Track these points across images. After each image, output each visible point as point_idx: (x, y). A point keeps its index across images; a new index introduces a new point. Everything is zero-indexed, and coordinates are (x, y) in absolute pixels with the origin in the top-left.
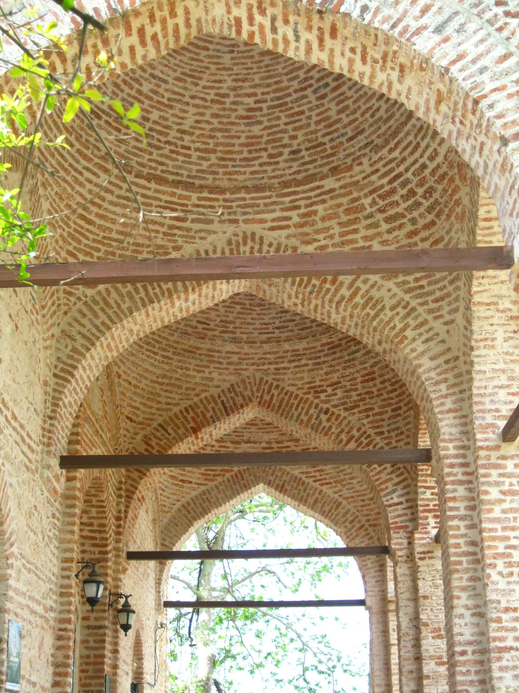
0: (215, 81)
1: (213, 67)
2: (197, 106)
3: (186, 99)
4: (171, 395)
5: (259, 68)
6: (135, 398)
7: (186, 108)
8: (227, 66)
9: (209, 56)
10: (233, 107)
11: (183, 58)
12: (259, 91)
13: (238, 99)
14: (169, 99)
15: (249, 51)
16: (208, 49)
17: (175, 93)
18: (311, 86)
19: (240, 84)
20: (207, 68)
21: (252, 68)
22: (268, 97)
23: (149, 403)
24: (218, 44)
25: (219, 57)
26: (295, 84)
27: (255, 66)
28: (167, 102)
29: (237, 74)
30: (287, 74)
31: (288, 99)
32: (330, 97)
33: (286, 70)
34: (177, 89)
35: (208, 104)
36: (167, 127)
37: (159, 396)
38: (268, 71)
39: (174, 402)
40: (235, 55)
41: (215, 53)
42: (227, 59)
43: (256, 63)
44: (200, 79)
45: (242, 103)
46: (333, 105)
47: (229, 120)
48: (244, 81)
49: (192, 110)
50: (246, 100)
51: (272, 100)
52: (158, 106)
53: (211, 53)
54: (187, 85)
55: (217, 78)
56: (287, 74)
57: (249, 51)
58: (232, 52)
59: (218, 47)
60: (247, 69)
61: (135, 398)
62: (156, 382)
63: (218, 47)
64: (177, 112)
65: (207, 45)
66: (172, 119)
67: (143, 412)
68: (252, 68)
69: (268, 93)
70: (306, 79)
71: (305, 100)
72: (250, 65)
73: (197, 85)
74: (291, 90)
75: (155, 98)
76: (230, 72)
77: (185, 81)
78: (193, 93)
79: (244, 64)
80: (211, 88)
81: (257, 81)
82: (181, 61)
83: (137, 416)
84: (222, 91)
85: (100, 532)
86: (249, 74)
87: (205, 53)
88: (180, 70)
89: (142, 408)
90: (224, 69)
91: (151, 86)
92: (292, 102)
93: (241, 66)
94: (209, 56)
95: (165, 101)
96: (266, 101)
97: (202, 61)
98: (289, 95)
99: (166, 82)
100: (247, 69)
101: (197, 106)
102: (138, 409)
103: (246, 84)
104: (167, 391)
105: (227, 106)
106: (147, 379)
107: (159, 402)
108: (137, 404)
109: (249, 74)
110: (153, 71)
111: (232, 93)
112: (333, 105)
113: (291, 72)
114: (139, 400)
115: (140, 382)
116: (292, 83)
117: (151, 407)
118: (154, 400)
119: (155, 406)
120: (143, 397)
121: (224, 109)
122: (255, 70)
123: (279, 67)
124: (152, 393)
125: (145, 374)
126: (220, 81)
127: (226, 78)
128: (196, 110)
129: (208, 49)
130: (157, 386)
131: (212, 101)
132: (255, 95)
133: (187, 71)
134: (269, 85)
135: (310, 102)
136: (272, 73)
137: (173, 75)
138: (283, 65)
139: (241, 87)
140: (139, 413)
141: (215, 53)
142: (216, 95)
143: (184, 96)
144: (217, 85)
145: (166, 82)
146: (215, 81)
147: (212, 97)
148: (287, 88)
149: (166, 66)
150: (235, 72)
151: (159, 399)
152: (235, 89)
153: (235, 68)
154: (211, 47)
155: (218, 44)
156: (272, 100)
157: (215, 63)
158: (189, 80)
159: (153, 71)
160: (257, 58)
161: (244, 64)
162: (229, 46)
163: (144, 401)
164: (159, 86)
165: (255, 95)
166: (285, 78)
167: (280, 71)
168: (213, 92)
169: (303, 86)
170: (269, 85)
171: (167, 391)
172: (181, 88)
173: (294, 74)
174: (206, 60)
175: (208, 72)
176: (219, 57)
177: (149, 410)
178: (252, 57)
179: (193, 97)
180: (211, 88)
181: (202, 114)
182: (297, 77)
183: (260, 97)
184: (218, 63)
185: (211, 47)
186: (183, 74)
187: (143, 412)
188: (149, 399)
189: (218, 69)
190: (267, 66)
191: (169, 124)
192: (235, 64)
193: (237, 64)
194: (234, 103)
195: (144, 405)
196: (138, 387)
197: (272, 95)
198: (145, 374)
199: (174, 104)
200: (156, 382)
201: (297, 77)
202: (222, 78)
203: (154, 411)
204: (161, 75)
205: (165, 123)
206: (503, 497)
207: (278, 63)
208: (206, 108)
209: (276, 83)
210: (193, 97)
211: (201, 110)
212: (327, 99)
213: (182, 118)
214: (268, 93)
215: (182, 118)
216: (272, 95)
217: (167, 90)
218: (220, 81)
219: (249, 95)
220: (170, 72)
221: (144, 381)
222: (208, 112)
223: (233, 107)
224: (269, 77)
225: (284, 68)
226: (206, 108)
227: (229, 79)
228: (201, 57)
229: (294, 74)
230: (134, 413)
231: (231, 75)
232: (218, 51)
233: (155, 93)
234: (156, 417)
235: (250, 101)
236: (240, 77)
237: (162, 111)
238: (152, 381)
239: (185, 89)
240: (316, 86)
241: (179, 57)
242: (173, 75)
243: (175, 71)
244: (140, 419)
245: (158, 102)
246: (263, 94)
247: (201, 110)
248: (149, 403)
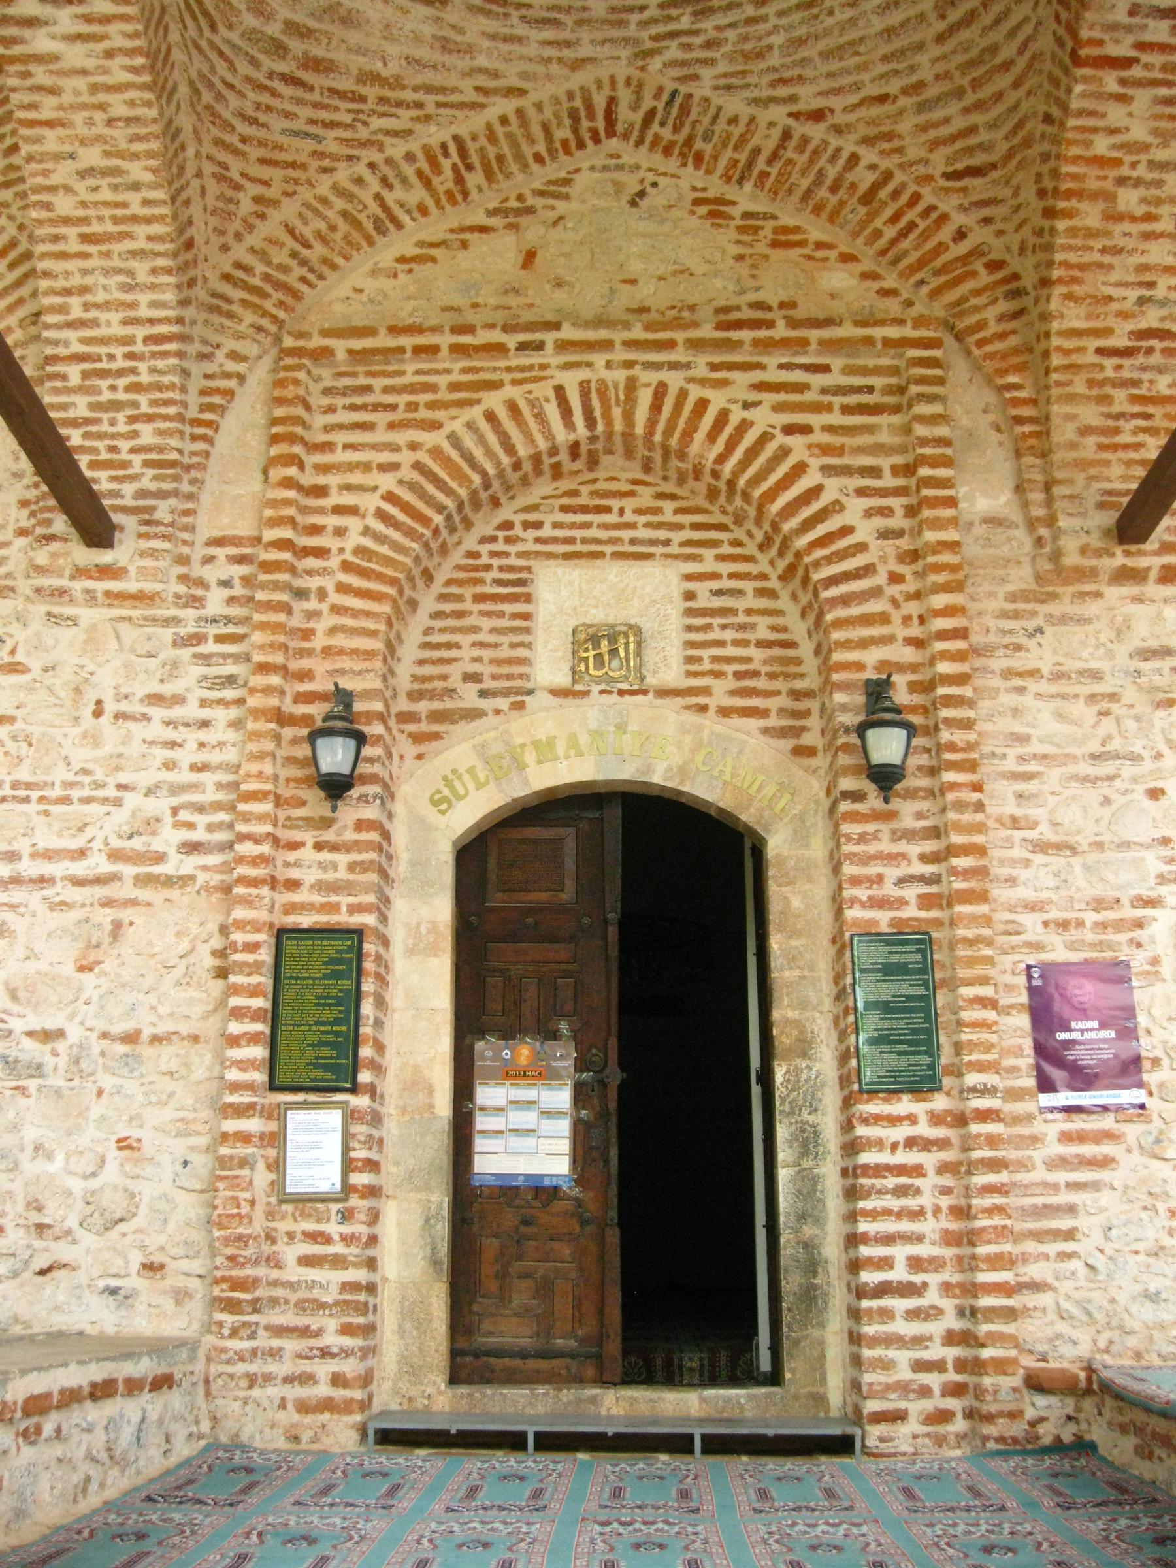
4: (1013, 21)
6: (937, 115)
23: (987, 91)
37: (993, 49)
39: (1028, 30)
47: (875, 892)
61: (937, 115)
62: (953, 29)
67: (993, 126)
83: (983, 147)
85: (808, 194)
89: (978, 118)
102: (972, 130)
104: (997, 22)
106: (920, 47)
107: (1007, 65)
108: (959, 123)
114: (953, 109)
115: (912, 69)
117: (999, 96)
118: (992, 72)
119: (1003, 81)
120: (959, 93)
124: (972, 64)
125: (898, 43)
130: (965, 35)
140: (983, 136)
151: (998, 60)
163: (970, 98)
171: (997, 22)
177: (1000, 108)
187: (993, 126)
188: (976, 84)
195: (979, 106)
196: (920, 86)
198: (898, 43)
200: (953, 29)
203: (1011, 97)
206: (482, 99)
221: (923, 59)
230: (969, 151)
234: (1025, 106)
238: (940, 38)
244: (1003, 147)
248: (987, 91)
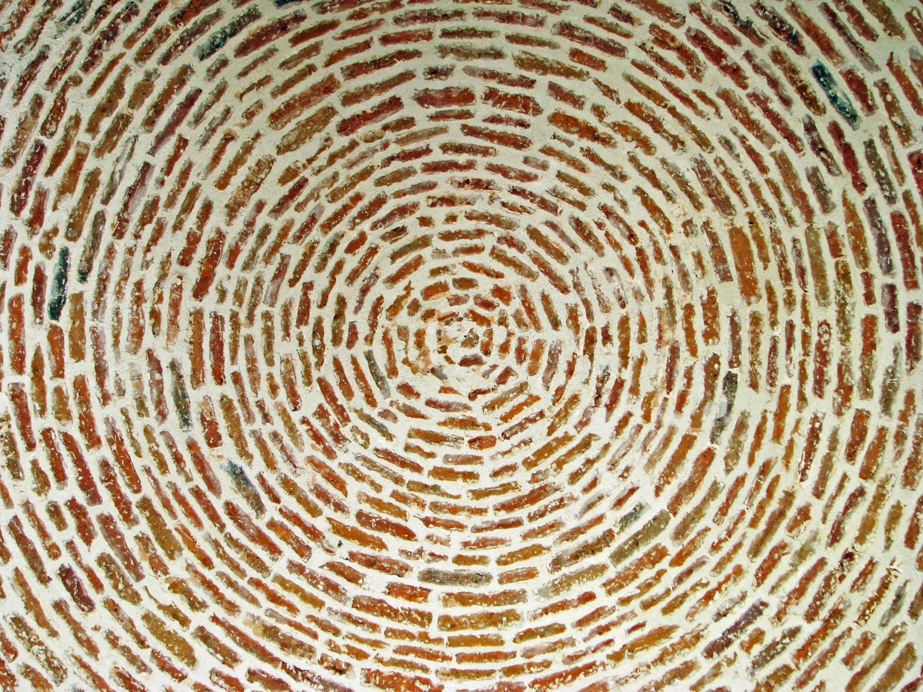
0: (810, 450)
1: (770, 450)
2: (867, 526)
3: (834, 557)
5: (790, 302)
7: (859, 565)
8: (773, 407)
9: (732, 457)
10: (898, 405)
11: (711, 538)
12: (859, 311)
13: (877, 384)
14: (810, 616)
15: (735, 327)
16: (708, 456)
17: (800, 591)
18: (836, 131)
19: (831, 371)
20: (765, 469)
21: (791, 326)
22: (880, 280)
24: (696, 421)
25: (741, 427)
26: (838, 185)
27: (783, 315)
28: (817, 625)
29: (803, 377)
30: (808, 213)
31: (885, 211)
32: (852, 61)
33: (796, 213)
34: (793, 583)
35: (871, 488)
36: (887, 646)
38: (802, 272)
40: (743, 378)
41: (726, 435)
42: (754, 403)
43: (774, 310)
44: (789, 497)
45: (891, 373)
46: (878, 50)
48: (823, 357)
49: (874, 547)
50: (883, 358)
51: (888, 269)
52: (813, 657)
53: (721, 450)
54: (796, 545)
55: (801, 443)
56: (808, 213)
57: (735, 327)
58: (731, 380)
59: (708, 422)
60: (790, 342)
63: (708, 422)
64: (858, 600)
65: (693, 454)
66: (872, 625)
68: (791, 326)
69: (868, 279)
70: (818, 147)
71: (882, 152)
72: (780, 332)
73: (804, 514)
74: (858, 200)
75: (785, 658)
76: (793, 399)
77: (781, 548)
78: (825, 531)
79: (774, 349)
80: (827, 465)
81: (831, 315)
82: (715, 547)
84: (845, 436)
86: (806, 337)
87: (718, 465)
88: (741, 558)
90: (780, 416)
91: (745, 661)
92: (891, 200)
93: (781, 361)
94: (732, 457)
95: (809, 629)
96: (892, 288)
97: (740, 481)
98: (871, 205)
99: (757, 610)
100: (790, 342)
101: (867, 526)
103: (835, 350)
105: (892, 424)
109: (806, 337)
110: (703, 644)
111: (857, 402)
112: (878, 50)
113: (799, 196)
116: (835, 198)
121: (900, 437)
122: (796, 317)
123: (786, 236)
126: (814, 435)
127: (807, 415)
128: (877, 536)
129: (708, 456)
131: (866, 473)
132: (870, 323)
133: (753, 534)
134: (844, 276)
135: (884, 135)
136: (807, 263)
137: (747, 581)
138: (780, 223)
139: (842, 370)
141: (726, 435)
142: (851, 456)
143: (822, 563)
144: (822, 448)
145: (757, 610)
146: (810, 450)
147: (854, 470)
148: (851, 215)
149: (709, 597)
150: (794, 383)
152: (845, 391)
153: (783, 379)
154: (702, 443)
155: (696, 421)
156: (888, 269)
157: (757, 445)
158: (781, 534)
159: (703, 644)
160: (762, 307)
161: (774, 349)
162: (710, 387)
164: (758, 636)
165: (870, 323)
166: (821, 220)
167: (799, 231)
168: (841, 465)
169: (839, 158)
170: (844, 276)
172: (795, 566)
173: (807, 187)
174: (741, 467)
175: (777, 469)
176: (741, 427)
178: (755, 320)
179: (836, 535)
180: (827, 465)
181: (895, 516)
182: (813, 176)
183: (878, 310)
184: (760, 433)
185: (702, 443)
186: (755, 551)
189: (778, 434)
190: (786, 277)
191: (882, 635)
192: (772, 381)
193: (772, 371)
194: (887, 402)
197: (874, 267)
199: (830, 603)
201: (813, 176)
202: (805, 428)
204: (728, 622)
205: (871, 651)
207: (777, 240)
208: (880, 498)
209: (836, 250)
210: (836, 535)
211: (883, 515)
212: (861, 72)
213: (884, 586)
214: (868, 279)
215: (884, 586)
216: (874, 267)
217: (779, 616)
218: (814, 435)
219: (869, 346)
220: (734, 590)
222: (896, 493)
223: (898, 405)
224: (820, 275)
225: (791, 221)
226: (880, 498)
227: (815, 405)
228: (727, 482)
229: (807, 187)
231: (802, 398)
232: (720, 425)
233: (771, 651)
235: (888, 342)
236: (810, 368)
237: (833, 650)
239: (802, 554)
240: (832, 114)
241: (703, 551)
242: (747, 581)
243: (738, 571)
245: (802, 653)
246: (869, 298)
247: (883, 515)
